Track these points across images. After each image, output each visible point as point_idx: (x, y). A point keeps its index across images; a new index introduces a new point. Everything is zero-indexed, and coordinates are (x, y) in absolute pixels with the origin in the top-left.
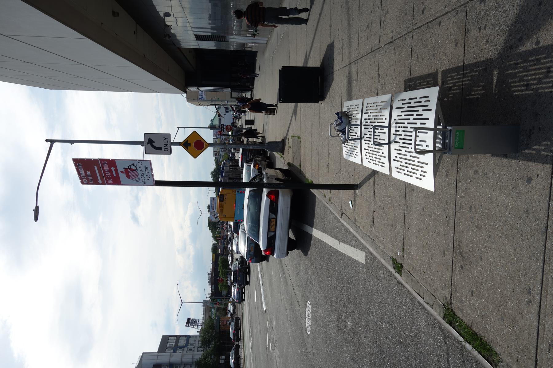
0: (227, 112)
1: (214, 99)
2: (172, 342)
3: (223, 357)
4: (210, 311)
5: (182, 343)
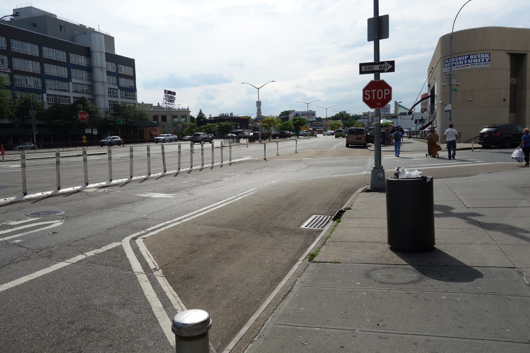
0: (416, 122)
1: (454, 82)
2: (124, 70)
3: (95, 132)
4: (183, 117)
5: (123, 82)
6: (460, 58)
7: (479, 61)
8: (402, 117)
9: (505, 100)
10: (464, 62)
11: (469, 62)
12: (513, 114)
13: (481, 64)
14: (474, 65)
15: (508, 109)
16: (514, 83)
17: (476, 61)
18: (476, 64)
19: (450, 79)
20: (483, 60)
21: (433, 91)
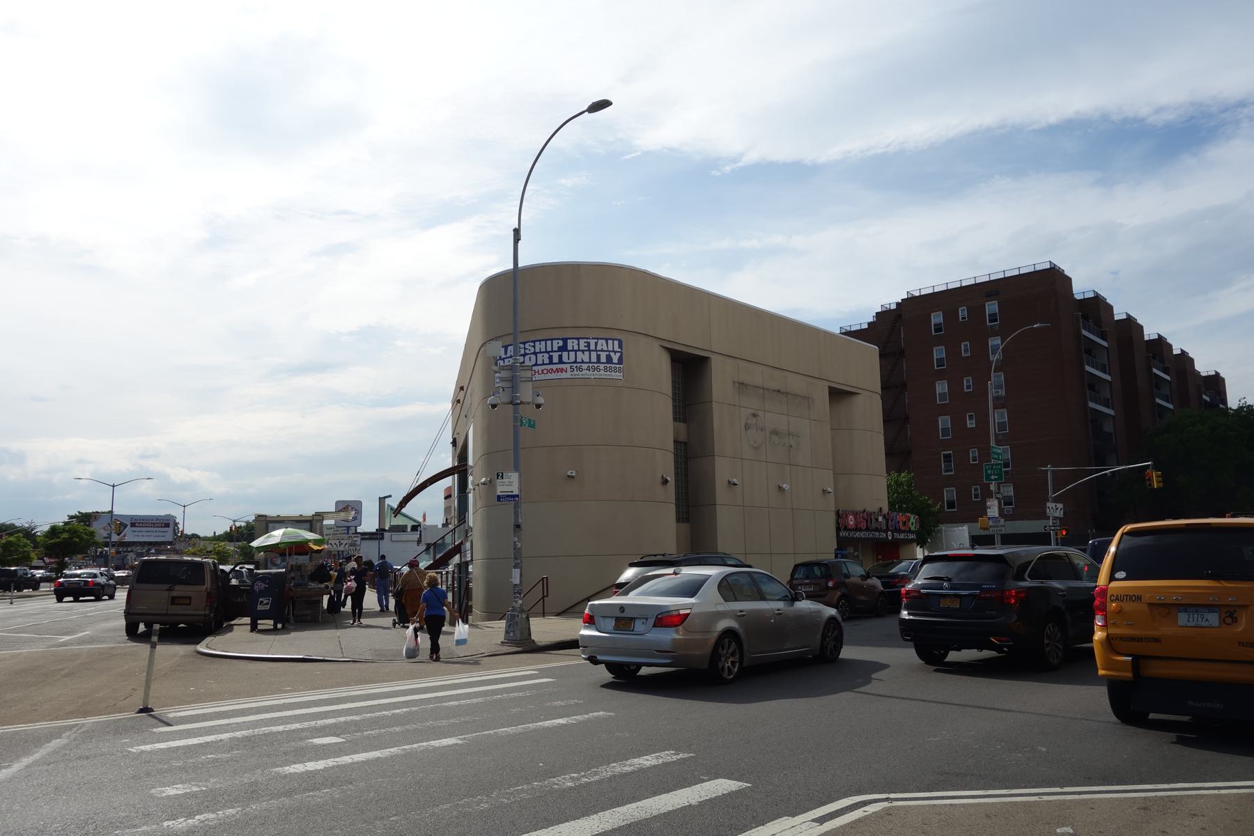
1: (526, 393)
6: (540, 346)
7: (594, 359)
8: (396, 536)
9: (665, 482)
10: (551, 358)
11: (565, 359)
12: (685, 526)
13: (597, 369)
14: (580, 369)
15: (670, 511)
16: (683, 438)
17: (586, 357)
18: (585, 366)
19: (513, 383)
20: (603, 359)
21: (462, 456)
